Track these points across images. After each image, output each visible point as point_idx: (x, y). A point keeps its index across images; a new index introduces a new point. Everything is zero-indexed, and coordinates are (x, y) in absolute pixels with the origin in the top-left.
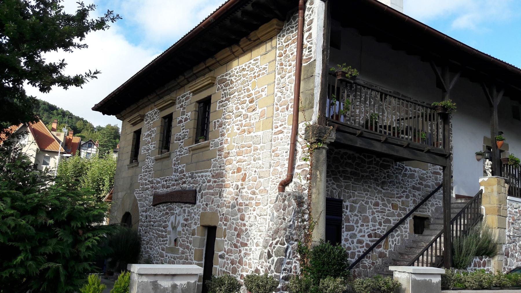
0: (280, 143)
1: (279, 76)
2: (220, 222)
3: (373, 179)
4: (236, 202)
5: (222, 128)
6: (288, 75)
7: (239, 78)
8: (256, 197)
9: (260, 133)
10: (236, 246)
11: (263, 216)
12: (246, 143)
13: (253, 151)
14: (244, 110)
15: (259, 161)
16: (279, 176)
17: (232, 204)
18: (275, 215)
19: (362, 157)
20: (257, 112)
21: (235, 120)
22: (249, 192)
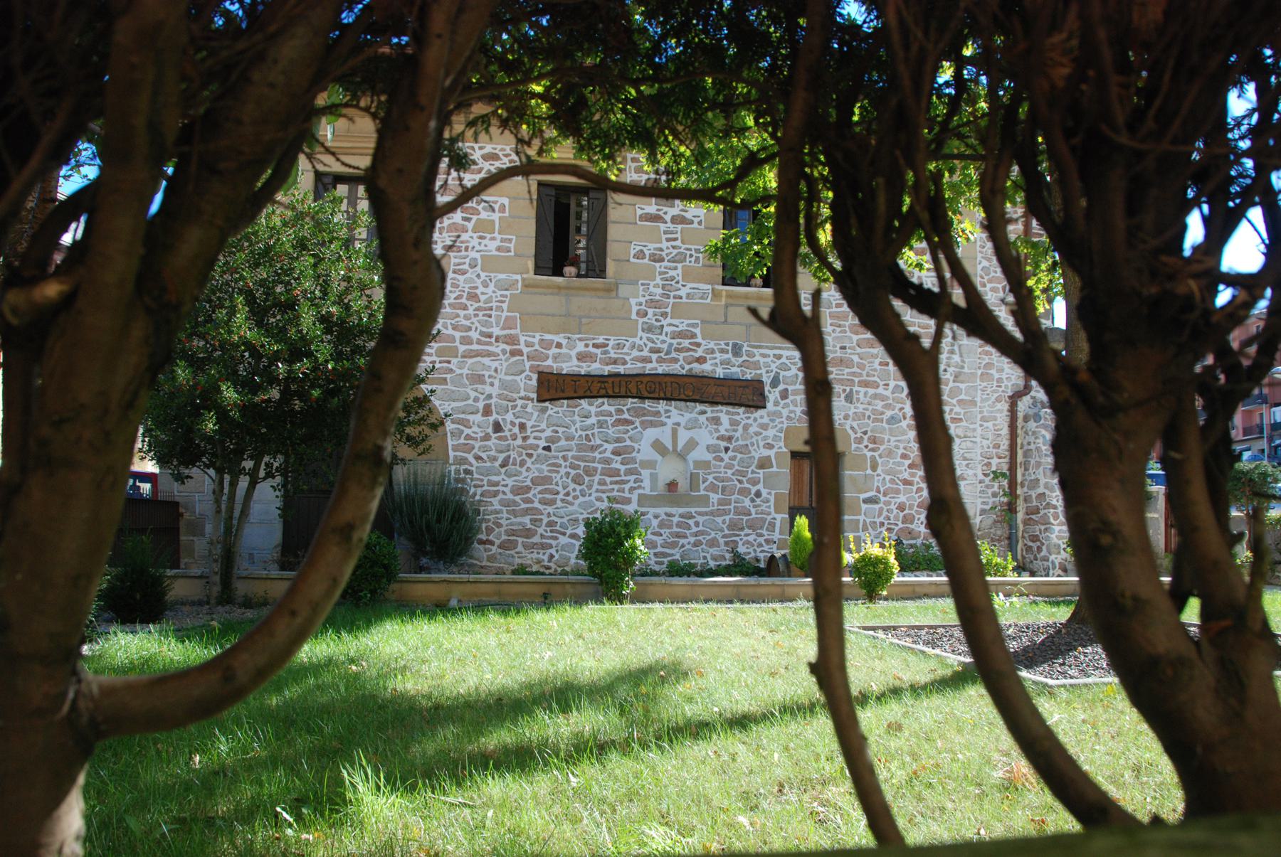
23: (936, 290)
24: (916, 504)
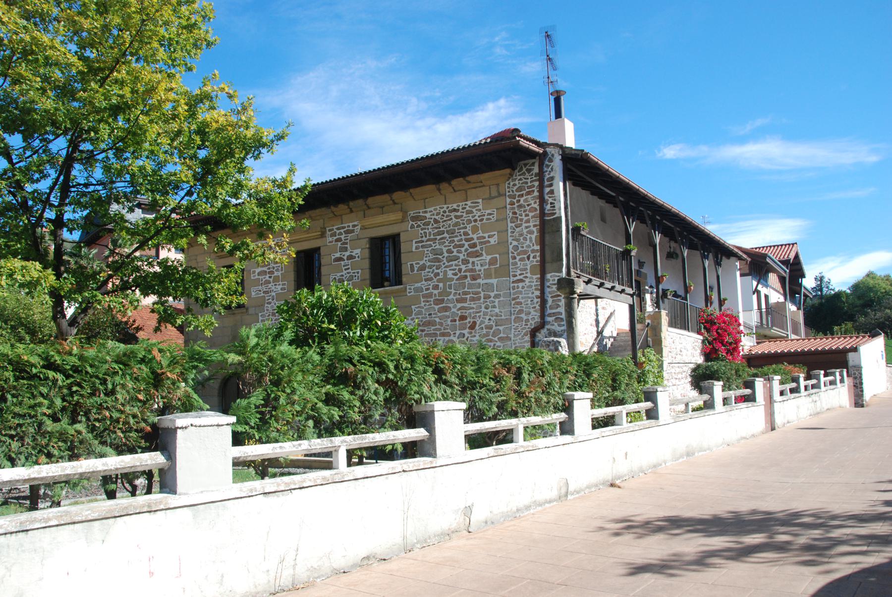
1: (513, 225)
6: (524, 225)
8: (494, 345)
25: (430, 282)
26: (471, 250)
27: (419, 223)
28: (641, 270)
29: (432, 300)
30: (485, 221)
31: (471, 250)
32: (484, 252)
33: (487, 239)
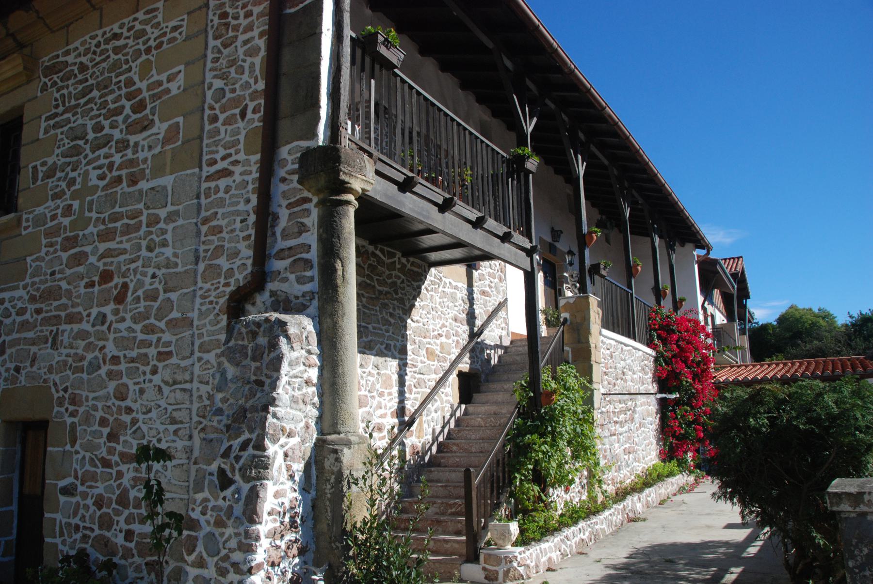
0: (223, 200)
1: (218, 42)
2: (56, 409)
3: (396, 299)
4: (100, 356)
5: (55, 179)
6: (242, 38)
7: (103, 57)
8: (159, 339)
9: (167, 181)
10: (106, 464)
11: (180, 383)
12: (123, 209)
13: (144, 225)
14: (118, 130)
15: (163, 250)
16: (222, 281)
17: (90, 363)
18: (229, 376)
19: (378, 252)
20: (154, 130)
21: (91, 156)
22: (138, 327)
23: (357, 48)
24: (114, 497)
25: (59, 201)
26: (134, 117)
27: (55, 77)
28: (556, 244)
29: (59, 239)
30: (165, 46)
31: (134, 117)
32: (156, 118)
33: (165, 85)
